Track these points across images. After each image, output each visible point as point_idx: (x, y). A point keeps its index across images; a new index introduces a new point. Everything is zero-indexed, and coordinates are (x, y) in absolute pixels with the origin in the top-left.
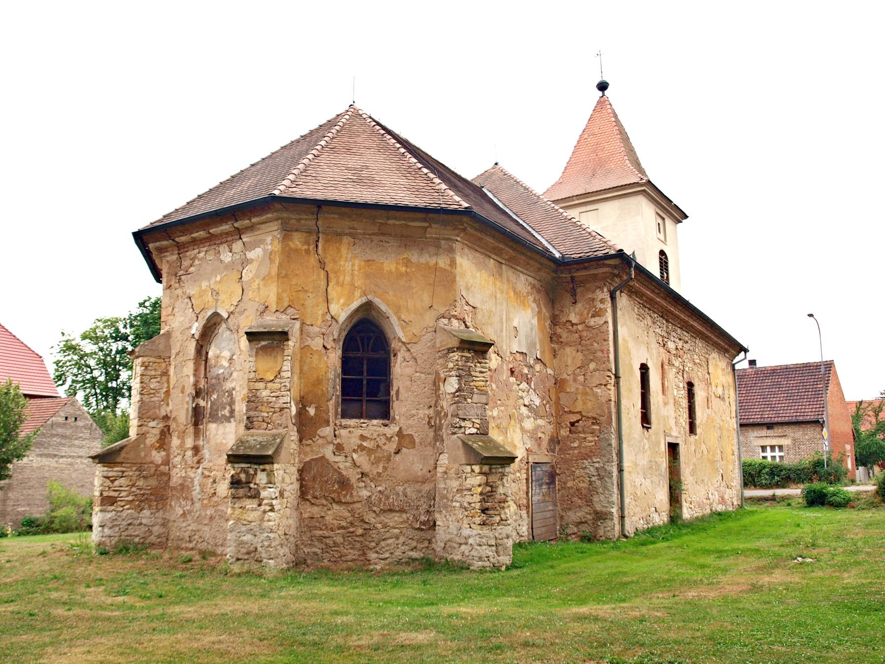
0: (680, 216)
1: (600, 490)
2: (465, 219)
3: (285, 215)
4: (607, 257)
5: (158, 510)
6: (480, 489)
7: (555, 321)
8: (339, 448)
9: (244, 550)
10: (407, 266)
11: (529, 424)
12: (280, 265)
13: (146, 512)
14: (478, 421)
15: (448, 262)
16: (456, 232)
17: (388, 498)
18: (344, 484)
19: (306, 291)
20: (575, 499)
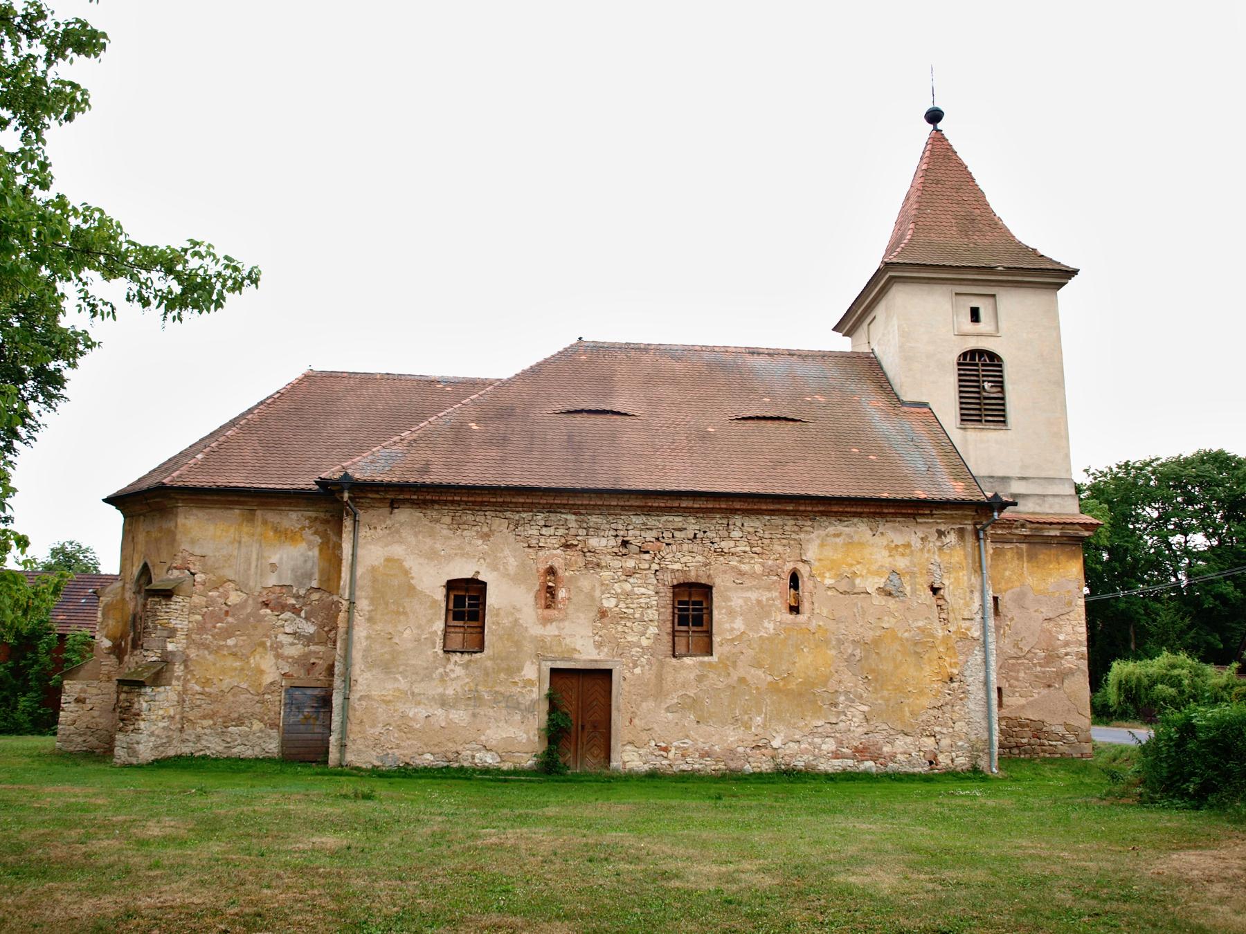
11: (295, 651)
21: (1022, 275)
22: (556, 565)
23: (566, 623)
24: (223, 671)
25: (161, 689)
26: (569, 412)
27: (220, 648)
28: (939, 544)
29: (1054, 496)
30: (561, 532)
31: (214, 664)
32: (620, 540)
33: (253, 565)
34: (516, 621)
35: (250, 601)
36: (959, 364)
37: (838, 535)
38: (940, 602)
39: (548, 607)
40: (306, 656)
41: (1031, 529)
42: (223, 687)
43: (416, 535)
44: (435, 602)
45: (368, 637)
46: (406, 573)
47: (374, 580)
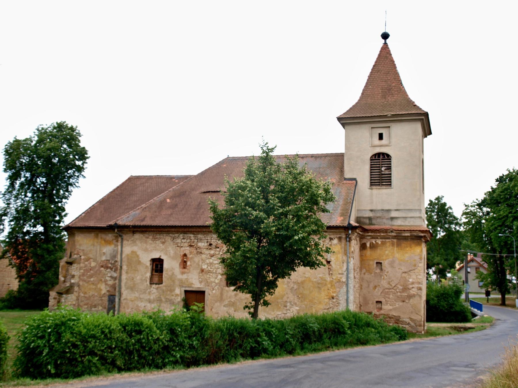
11: (111, 282)
21: (396, 117)
22: (187, 253)
23: (190, 274)
24: (90, 289)
25: (70, 295)
26: (204, 192)
28: (330, 243)
29: (411, 217)
30: (188, 241)
32: (209, 243)
34: (173, 273)
36: (371, 160)
38: (330, 267)
39: (184, 268)
41: (396, 233)
43: (141, 243)
44: (147, 267)
45: (126, 279)
46: (138, 256)
47: (128, 259)
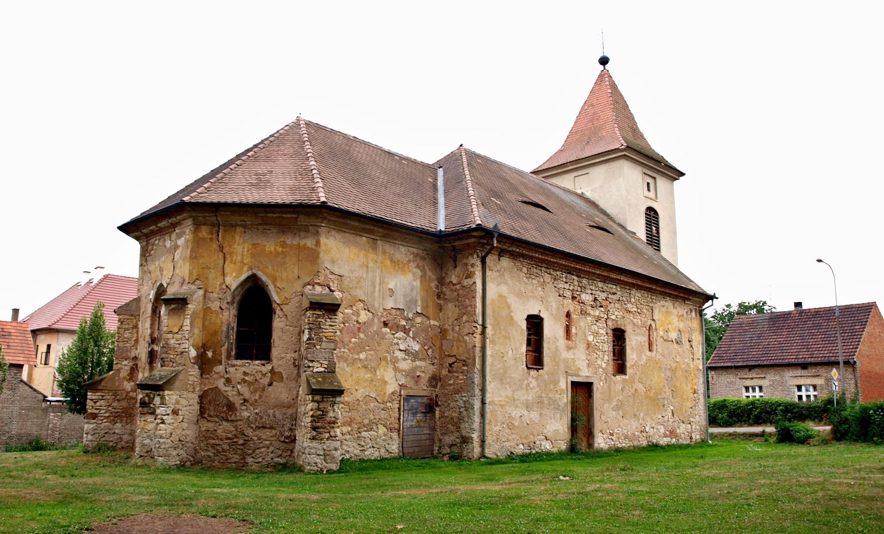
0: (675, 174)
1: (466, 419)
2: (324, 210)
3: (194, 214)
4: (470, 230)
5: (127, 423)
6: (311, 413)
7: (441, 281)
8: (228, 381)
9: (145, 450)
10: (283, 247)
11: (405, 365)
12: (192, 250)
13: (118, 425)
14: (326, 362)
15: (314, 242)
16: (320, 220)
17: (261, 418)
18: (231, 407)
19: (209, 268)
20: (450, 426)
23: (576, 351)
27: (355, 361)
31: (351, 376)
33: (377, 289)
34: (557, 347)
35: (376, 320)
37: (663, 306)
40: (415, 369)
42: (359, 397)
46: (509, 307)
